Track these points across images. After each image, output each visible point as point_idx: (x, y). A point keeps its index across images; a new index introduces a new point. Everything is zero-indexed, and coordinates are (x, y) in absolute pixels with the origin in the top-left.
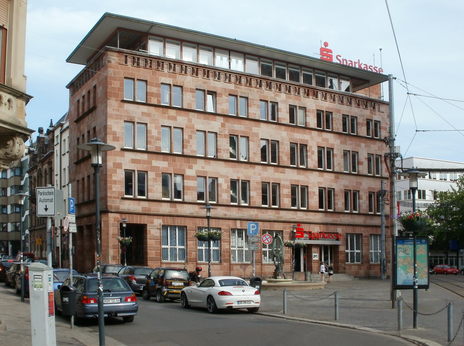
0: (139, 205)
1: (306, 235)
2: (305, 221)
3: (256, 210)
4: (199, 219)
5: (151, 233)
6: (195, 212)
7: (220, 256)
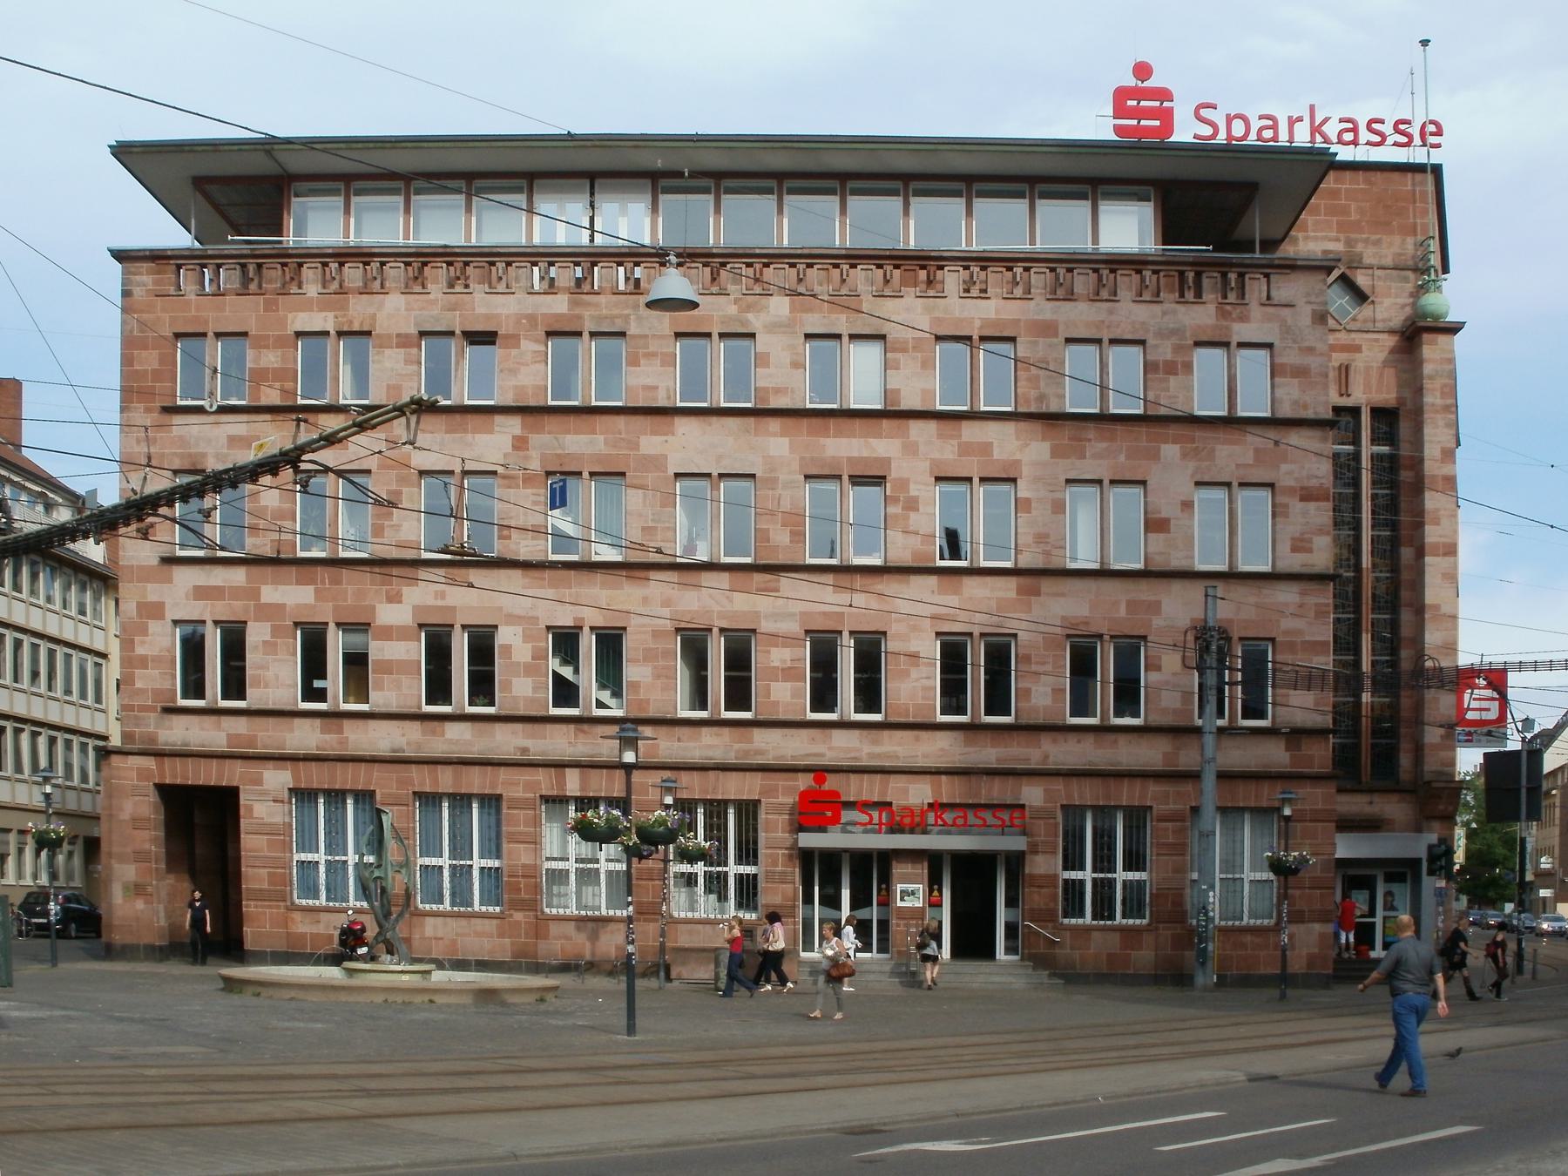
0: (219, 728)
2: (865, 762)
6: (408, 744)
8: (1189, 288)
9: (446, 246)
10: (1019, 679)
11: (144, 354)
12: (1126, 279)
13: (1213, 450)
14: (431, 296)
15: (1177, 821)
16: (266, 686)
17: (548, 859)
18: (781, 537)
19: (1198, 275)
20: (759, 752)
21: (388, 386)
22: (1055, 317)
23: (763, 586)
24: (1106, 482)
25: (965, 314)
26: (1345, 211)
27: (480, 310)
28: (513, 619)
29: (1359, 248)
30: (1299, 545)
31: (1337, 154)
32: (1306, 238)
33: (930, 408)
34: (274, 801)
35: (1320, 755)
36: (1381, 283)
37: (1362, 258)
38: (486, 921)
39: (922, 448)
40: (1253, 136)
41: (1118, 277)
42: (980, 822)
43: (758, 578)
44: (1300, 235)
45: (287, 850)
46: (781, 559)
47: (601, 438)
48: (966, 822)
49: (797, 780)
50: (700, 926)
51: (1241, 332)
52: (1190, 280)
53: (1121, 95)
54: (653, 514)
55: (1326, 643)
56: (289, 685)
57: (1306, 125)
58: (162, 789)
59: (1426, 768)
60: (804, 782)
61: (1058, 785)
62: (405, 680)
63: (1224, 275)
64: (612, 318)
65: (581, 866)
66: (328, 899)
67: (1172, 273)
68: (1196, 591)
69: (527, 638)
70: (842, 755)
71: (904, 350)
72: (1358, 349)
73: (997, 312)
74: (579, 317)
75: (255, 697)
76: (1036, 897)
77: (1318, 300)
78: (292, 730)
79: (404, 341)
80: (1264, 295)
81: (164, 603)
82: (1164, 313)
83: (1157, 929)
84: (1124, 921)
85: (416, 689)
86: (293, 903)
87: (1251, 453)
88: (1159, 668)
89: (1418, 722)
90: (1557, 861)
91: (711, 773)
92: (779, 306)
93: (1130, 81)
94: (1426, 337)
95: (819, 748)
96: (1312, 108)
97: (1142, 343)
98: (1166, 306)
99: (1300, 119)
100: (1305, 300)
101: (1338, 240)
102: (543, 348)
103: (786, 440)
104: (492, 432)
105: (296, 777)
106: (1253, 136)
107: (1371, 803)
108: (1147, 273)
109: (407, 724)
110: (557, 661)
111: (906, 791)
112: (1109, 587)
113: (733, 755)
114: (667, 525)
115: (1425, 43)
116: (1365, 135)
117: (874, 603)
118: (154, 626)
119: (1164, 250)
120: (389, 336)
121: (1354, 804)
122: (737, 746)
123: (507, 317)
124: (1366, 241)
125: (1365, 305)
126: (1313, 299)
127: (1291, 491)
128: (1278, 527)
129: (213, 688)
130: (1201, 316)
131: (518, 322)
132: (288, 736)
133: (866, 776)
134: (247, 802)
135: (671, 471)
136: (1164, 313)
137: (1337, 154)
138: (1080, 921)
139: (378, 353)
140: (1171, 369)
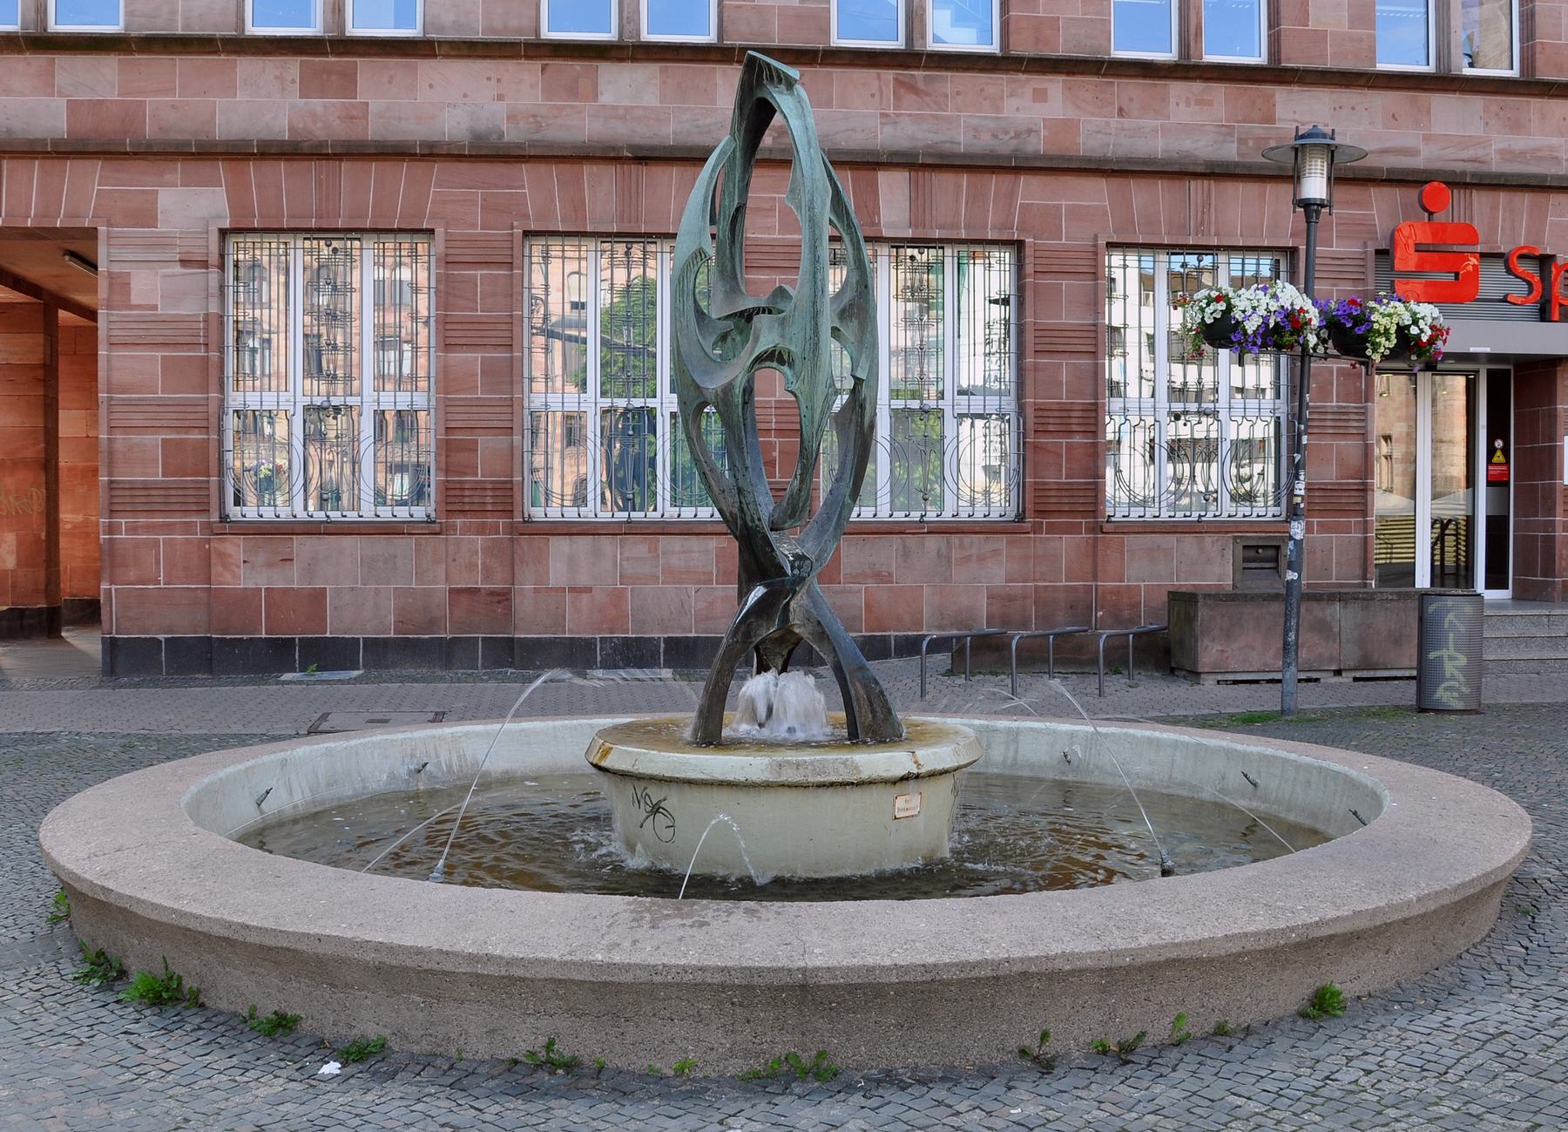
0: (49, 88)
1: (1493, 281)
2: (1497, 166)
3: (1055, 85)
4: (542, 168)
5: (135, 300)
6: (511, 118)
7: (959, 336)
38: (694, 543)
49: (1366, 204)
50: (1172, 539)
70: (1451, 153)
78: (230, 90)
86: (224, 518)
91: (1195, 186)
132: (220, 102)
133: (1502, 197)
134: (116, 268)
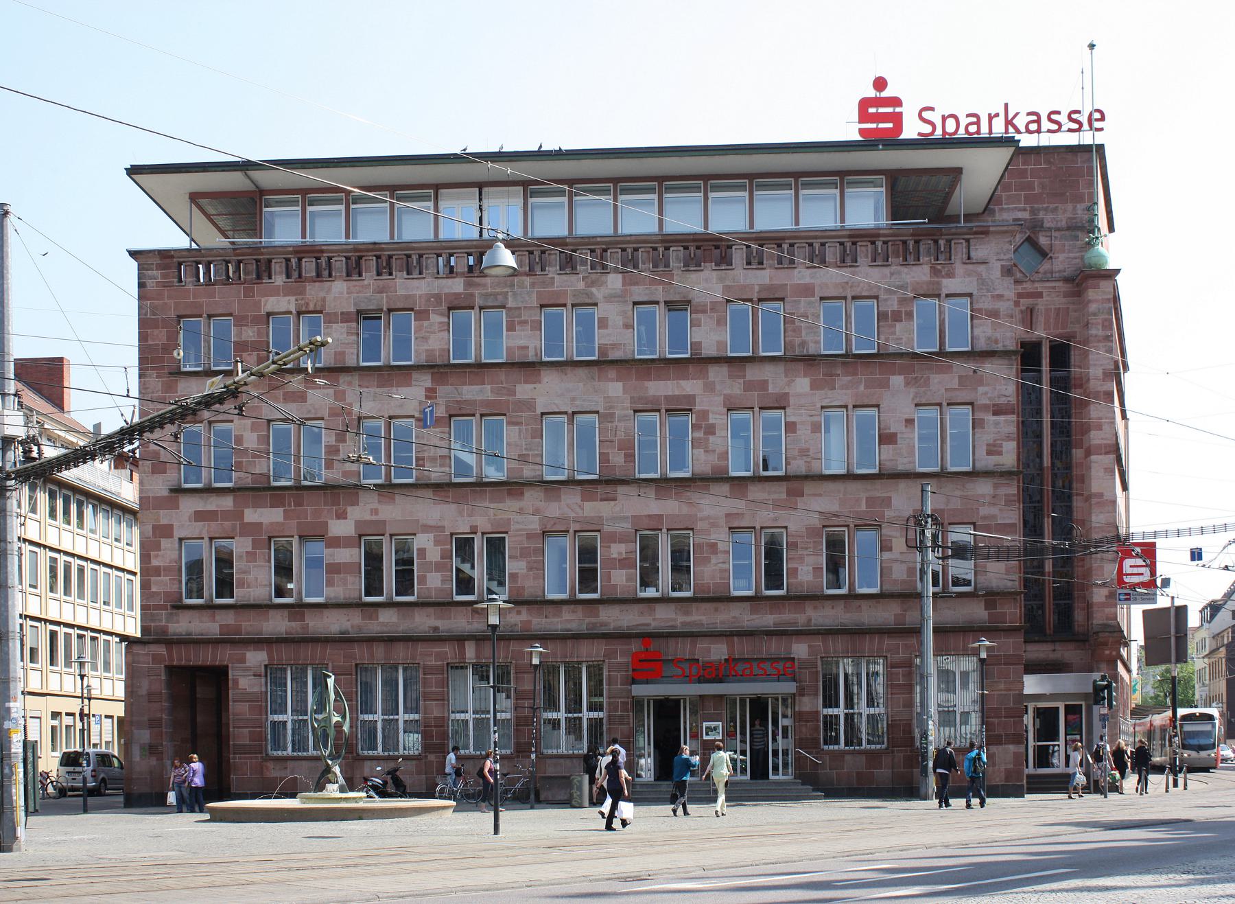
0: (214, 621)
6: (352, 627)
8: (910, 253)
9: (375, 243)
10: (789, 561)
11: (156, 332)
12: (863, 249)
13: (928, 378)
14: (366, 282)
15: (905, 667)
16: (248, 587)
17: (453, 712)
18: (618, 459)
19: (917, 242)
20: (602, 624)
21: (335, 352)
22: (812, 281)
23: (604, 496)
24: (850, 407)
25: (748, 282)
26: (1030, 186)
27: (401, 292)
28: (426, 528)
29: (1041, 215)
30: (993, 450)
31: (1019, 141)
32: (1002, 210)
33: (723, 354)
34: (255, 675)
35: (1013, 613)
36: (1057, 242)
37: (1043, 223)
39: (718, 387)
40: (962, 131)
41: (858, 248)
42: (763, 672)
43: (601, 490)
44: (996, 208)
45: (264, 713)
46: (618, 474)
47: (489, 387)
48: (752, 672)
51: (949, 285)
52: (911, 247)
53: (865, 104)
54: (526, 445)
55: (1014, 525)
56: (266, 585)
57: (1001, 119)
58: (172, 670)
59: (1095, 622)
60: (635, 646)
61: (818, 642)
62: (349, 578)
63: (936, 242)
64: (495, 295)
65: (477, 716)
66: (293, 750)
67: (898, 243)
68: (914, 488)
69: (437, 542)
71: (704, 311)
72: (1040, 295)
73: (771, 279)
74: (472, 295)
75: (240, 595)
76: (804, 730)
77: (1005, 257)
79: (345, 318)
80: (965, 256)
81: (172, 525)
82: (892, 274)
83: (893, 752)
84: (868, 747)
85: (354, 586)
87: (956, 380)
88: (890, 549)
89: (1086, 587)
90: (1225, 706)
92: (614, 281)
93: (872, 93)
94: (1091, 282)
95: (646, 619)
96: (1006, 105)
97: (876, 297)
98: (893, 268)
99: (997, 115)
100: (995, 258)
101: (1025, 210)
102: (446, 320)
103: (620, 384)
104: (409, 385)
105: (270, 657)
106: (962, 131)
107: (1054, 650)
108: (879, 244)
109: (351, 611)
110: (330, 787)
111: (709, 650)
112: (853, 486)
113: (584, 627)
114: (536, 452)
115: (1092, 46)
116: (1046, 125)
117: (685, 510)
118: (165, 543)
119: (892, 224)
120: (335, 314)
121: (1039, 651)
122: (587, 620)
123: (420, 296)
124: (1046, 209)
125: (1046, 260)
126: (1002, 256)
127: (985, 408)
128: (977, 436)
129: (209, 589)
130: (919, 274)
131: (429, 300)
132: (265, 624)
135: (539, 411)
136: (892, 274)
137: (1019, 141)
138: (836, 747)
139: (328, 327)
140: (897, 316)
